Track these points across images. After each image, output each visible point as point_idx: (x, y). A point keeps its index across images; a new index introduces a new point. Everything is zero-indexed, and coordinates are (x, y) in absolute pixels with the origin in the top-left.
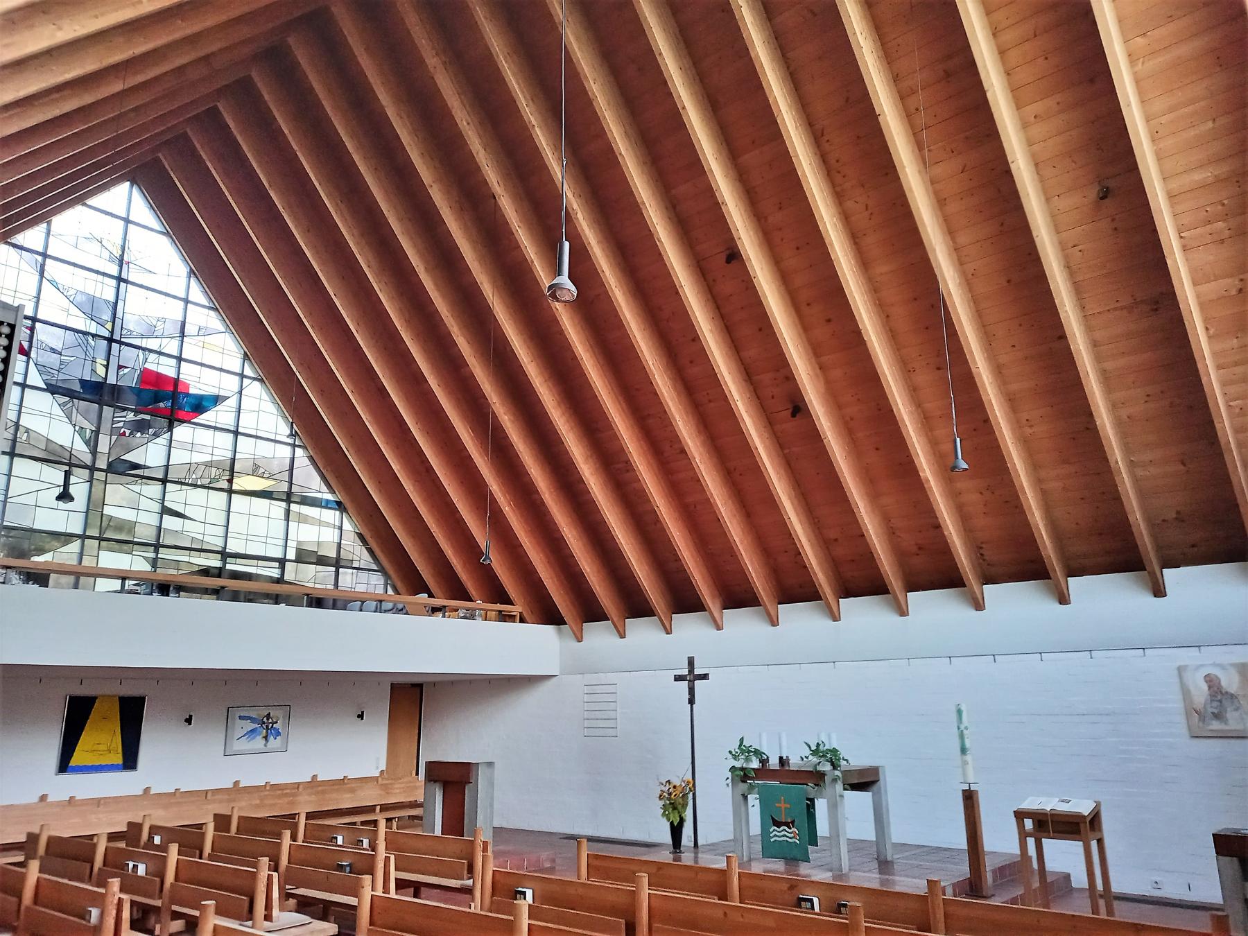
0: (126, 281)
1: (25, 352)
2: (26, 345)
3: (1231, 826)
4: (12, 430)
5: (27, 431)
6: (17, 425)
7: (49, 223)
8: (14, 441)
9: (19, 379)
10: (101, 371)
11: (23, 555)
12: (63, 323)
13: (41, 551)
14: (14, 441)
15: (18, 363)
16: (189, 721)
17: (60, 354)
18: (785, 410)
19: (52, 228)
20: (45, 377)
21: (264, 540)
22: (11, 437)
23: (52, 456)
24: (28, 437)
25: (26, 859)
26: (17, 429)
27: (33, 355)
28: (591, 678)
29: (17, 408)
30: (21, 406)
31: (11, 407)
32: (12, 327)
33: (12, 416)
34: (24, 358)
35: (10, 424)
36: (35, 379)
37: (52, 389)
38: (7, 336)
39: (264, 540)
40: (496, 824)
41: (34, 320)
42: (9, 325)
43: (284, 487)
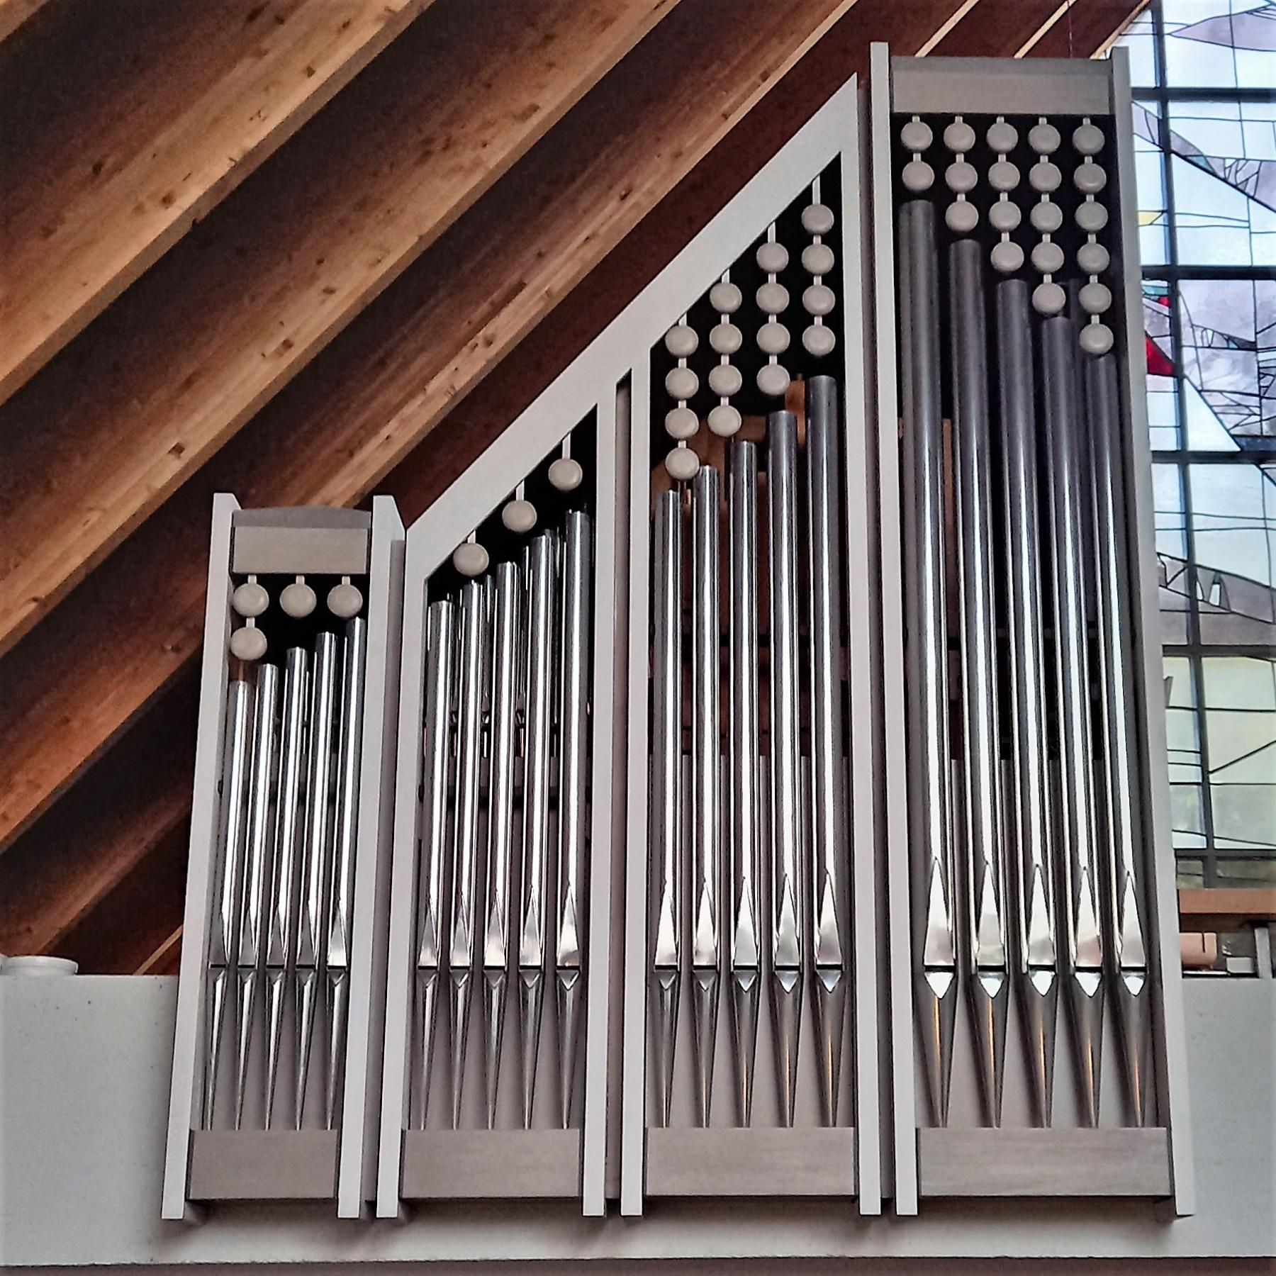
0: (1258, 396)
1: (1165, 365)
2: (1165, 345)
4: (1180, 584)
5: (1218, 577)
6: (1190, 565)
8: (1193, 611)
9: (1168, 442)
12: (1242, 261)
14: (1193, 611)
17: (1251, 347)
20: (1230, 420)
21: (1261, 524)
22: (1181, 602)
26: (1192, 581)
27: (1191, 372)
28: (423, 137)
29: (1178, 521)
30: (1187, 513)
31: (1160, 521)
32: (1106, 124)
33: (1171, 545)
34: (1169, 382)
38: (1106, 318)
39: (1261, 524)
40: (1153, 448)
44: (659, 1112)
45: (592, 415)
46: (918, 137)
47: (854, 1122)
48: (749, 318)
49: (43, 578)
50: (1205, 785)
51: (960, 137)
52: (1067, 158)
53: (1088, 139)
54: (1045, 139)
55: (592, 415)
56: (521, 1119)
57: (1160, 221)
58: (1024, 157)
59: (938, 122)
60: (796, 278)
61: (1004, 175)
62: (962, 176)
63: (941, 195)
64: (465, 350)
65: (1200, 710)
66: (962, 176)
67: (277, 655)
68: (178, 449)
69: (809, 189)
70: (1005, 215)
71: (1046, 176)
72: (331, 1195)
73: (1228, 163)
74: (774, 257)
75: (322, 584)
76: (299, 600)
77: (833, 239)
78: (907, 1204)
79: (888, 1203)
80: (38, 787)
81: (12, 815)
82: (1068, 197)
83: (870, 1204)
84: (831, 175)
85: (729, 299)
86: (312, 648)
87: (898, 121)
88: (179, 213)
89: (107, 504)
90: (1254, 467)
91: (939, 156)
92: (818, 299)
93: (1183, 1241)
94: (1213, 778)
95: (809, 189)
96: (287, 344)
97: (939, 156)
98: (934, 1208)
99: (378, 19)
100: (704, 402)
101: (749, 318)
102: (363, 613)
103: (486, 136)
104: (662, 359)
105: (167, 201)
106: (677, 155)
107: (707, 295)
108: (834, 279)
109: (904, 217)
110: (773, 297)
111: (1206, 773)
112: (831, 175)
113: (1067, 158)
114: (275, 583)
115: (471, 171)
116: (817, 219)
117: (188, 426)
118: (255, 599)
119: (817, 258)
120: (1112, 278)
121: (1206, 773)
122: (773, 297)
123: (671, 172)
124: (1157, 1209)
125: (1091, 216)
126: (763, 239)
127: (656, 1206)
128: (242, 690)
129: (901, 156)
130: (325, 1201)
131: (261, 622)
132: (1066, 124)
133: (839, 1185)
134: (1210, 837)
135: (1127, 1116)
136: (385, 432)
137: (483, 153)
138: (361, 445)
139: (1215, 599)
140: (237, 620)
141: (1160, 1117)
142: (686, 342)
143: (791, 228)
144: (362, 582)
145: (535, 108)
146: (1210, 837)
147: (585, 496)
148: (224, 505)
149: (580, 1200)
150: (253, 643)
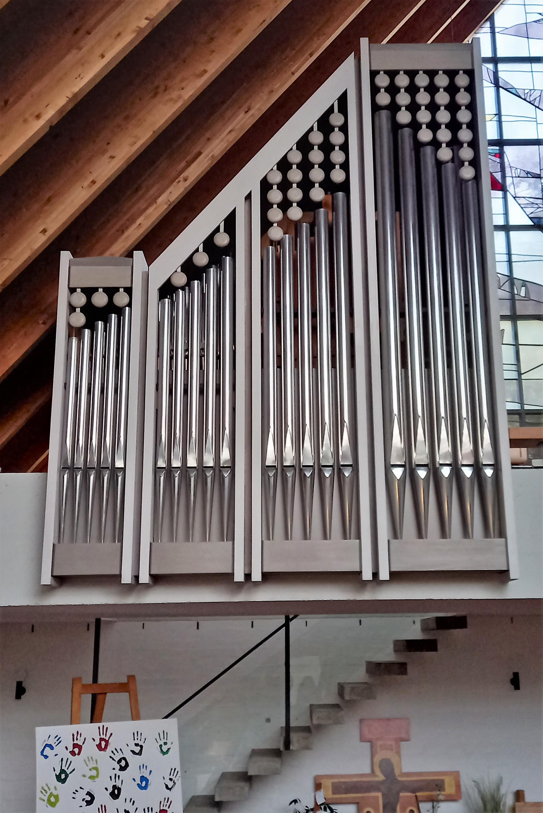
1: (499, 186)
2: (498, 176)
3: (155, 623)
4: (507, 287)
5: (525, 283)
6: (511, 279)
7: (491, 19)
8: (513, 300)
9: (499, 221)
15: (495, 202)
16: (515, 682)
18: (187, 373)
19: (497, 24)
20: (529, 210)
22: (507, 295)
24: (527, 291)
25: (120, 766)
26: (512, 285)
27: (511, 189)
30: (509, 254)
32: (470, 73)
34: (500, 194)
35: (503, 279)
36: (518, 217)
41: (495, 60)
42: (466, 72)
43: (435, 804)
44: (396, 532)
46: (383, 81)
47: (359, 537)
48: (306, 166)
50: (519, 380)
51: (402, 81)
52: (452, 89)
53: (462, 81)
54: (442, 81)
58: (432, 89)
59: (392, 74)
60: (327, 147)
61: (423, 98)
62: (403, 99)
64: (175, 183)
65: (516, 345)
66: (403, 99)
67: (91, 325)
68: (44, 231)
71: (442, 98)
72: (118, 573)
74: (317, 138)
75: (111, 292)
76: (100, 300)
77: (344, 129)
78: (384, 575)
84: (343, 100)
85: (296, 157)
86: (107, 321)
87: (374, 74)
89: (12, 256)
91: (393, 90)
92: (337, 157)
93: (514, 591)
96: (94, 182)
97: (393, 90)
99: (133, 31)
100: (285, 205)
101: (306, 166)
102: (130, 305)
103: (183, 85)
104: (266, 186)
105: (38, 117)
107: (285, 156)
108: (345, 147)
112: (343, 100)
113: (452, 89)
114: (89, 292)
115: (176, 101)
116: (336, 119)
118: (80, 299)
120: (474, 144)
122: (316, 156)
124: (501, 576)
125: (463, 98)
127: (267, 577)
128: (74, 341)
129: (375, 90)
131: (83, 310)
132: (452, 74)
133: (351, 566)
135: (487, 533)
136: (138, 221)
139: (523, 294)
141: (502, 534)
143: (324, 124)
144: (129, 291)
145: (205, 71)
148: (65, 256)
149: (120, 576)
150: (79, 319)
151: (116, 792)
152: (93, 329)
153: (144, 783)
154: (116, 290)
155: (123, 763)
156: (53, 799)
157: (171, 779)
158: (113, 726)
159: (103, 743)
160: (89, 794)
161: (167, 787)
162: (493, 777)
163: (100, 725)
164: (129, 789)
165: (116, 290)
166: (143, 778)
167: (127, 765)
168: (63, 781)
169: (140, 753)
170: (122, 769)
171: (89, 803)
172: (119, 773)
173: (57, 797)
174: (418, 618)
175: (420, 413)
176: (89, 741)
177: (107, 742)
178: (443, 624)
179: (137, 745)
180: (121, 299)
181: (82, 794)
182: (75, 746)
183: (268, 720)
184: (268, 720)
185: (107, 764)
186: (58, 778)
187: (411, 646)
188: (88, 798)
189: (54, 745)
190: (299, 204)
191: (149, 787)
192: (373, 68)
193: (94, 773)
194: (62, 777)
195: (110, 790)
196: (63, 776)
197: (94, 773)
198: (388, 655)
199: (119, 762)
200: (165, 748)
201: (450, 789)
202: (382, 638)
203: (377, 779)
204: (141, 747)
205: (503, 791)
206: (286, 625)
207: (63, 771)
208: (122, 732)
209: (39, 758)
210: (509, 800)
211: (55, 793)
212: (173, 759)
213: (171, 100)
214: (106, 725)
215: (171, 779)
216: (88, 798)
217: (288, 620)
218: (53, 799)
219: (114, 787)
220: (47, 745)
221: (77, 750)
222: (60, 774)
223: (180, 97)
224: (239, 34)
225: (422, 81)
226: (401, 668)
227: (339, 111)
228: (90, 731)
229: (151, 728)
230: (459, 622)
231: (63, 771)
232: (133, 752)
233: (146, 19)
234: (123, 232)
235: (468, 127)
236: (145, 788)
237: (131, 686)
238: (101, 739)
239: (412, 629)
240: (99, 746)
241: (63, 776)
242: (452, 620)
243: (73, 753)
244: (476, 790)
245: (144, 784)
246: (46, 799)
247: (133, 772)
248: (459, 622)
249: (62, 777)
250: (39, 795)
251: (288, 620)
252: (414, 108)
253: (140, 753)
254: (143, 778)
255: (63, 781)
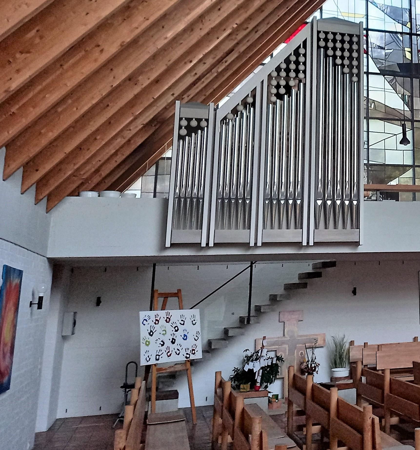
10: (408, 55)
11: (382, 181)
13: (392, 178)
16: (354, 292)
23: (389, 116)
32: (358, 36)
36: (373, 68)
37: (383, 72)
45: (256, 88)
46: (322, 36)
47: (302, 228)
48: (288, 70)
49: (144, 120)
50: (368, 149)
51: (330, 37)
52: (351, 43)
53: (355, 39)
55: (256, 88)
56: (237, 228)
57: (365, 17)
58: (342, 42)
59: (326, 33)
60: (297, 63)
61: (339, 45)
62: (330, 44)
63: (326, 48)
64: (221, 63)
65: (368, 132)
66: (330, 44)
68: (173, 94)
69: (300, 45)
70: (338, 53)
72: (248, 242)
73: (381, 5)
74: (293, 58)
75: (199, 120)
76: (194, 123)
77: (305, 55)
79: (207, 244)
80: (123, 155)
81: (118, 161)
82: (351, 50)
83: (204, 244)
84: (305, 42)
85: (284, 66)
86: (196, 133)
87: (319, 32)
88: (193, 64)
89: (158, 105)
90: (382, 76)
92: (301, 67)
93: (360, 249)
94: (370, 147)
95: (300, 45)
96: (196, 74)
97: (326, 40)
98: (316, 244)
99: (231, 29)
100: (278, 87)
101: (288, 70)
102: (207, 127)
103: (238, 33)
105: (191, 62)
106: (268, 23)
107: (279, 65)
108: (305, 64)
109: (319, 51)
110: (293, 66)
111: (368, 146)
112: (305, 42)
113: (351, 43)
114: (189, 120)
115: (234, 40)
116: (302, 51)
117: (175, 90)
118: (184, 123)
119: (302, 59)
121: (368, 146)
122: (293, 66)
123: (267, 27)
125: (355, 63)
126: (291, 54)
127: (173, 245)
128: (181, 141)
129: (319, 39)
130: (248, 243)
131: (186, 127)
132: (351, 36)
133: (298, 240)
134: (368, 161)
135: (352, 227)
136: (202, 80)
137: (237, 37)
138: (197, 83)
139: (373, 107)
140: (180, 127)
141: (358, 227)
142: (275, 74)
143: (296, 52)
144: (207, 120)
145: (247, 28)
146: (368, 161)
147: (253, 104)
148: (178, 103)
149: (201, 243)
150: (184, 132)
151: (174, 341)
152: (190, 136)
153: (185, 338)
154: (201, 120)
155: (176, 328)
156: (147, 343)
157: (197, 336)
158: (172, 312)
159: (168, 319)
160: (162, 341)
161: (195, 340)
162: (341, 336)
163: (167, 311)
164: (179, 340)
165: (201, 120)
166: (185, 335)
167: (178, 329)
168: (152, 335)
169: (183, 324)
170: (176, 331)
171: (162, 345)
172: (175, 333)
173: (149, 342)
174: (311, 262)
175: (330, 179)
176: (162, 318)
177: (169, 319)
178: (325, 265)
179: (182, 320)
180: (204, 124)
181: (159, 342)
182: (156, 320)
183: (233, 314)
184: (233, 314)
185: (170, 329)
186: (149, 334)
187: (309, 275)
188: (162, 343)
189: (147, 320)
190: (284, 87)
191: (187, 339)
192: (319, 30)
193: (164, 332)
194: (151, 334)
195: (171, 340)
196: (151, 333)
197: (164, 332)
198: (280, 291)
199: (175, 328)
200: (194, 322)
201: (320, 342)
202: (293, 272)
203: (286, 339)
204: (184, 321)
205: (345, 341)
206: (251, 266)
207: (151, 331)
208: (176, 314)
209: (141, 325)
210: (347, 346)
211: (148, 340)
212: (198, 327)
213: (232, 39)
214: (169, 311)
215: (197, 336)
216: (162, 343)
217: (252, 263)
218: (147, 343)
219: (173, 339)
220: (145, 320)
221: (157, 322)
222: (150, 332)
223: (236, 38)
224: (263, 12)
225: (339, 37)
226: (305, 285)
227: (303, 47)
228: (162, 314)
229: (187, 313)
230: (333, 264)
231: (151, 331)
232: (180, 323)
233: (236, 24)
234: (195, 85)
235: (356, 51)
236: (186, 339)
237: (179, 295)
238: (167, 318)
239: (307, 267)
240: (166, 321)
241: (151, 333)
242: (329, 263)
243: (155, 323)
244: (333, 341)
245: (185, 338)
246: (144, 342)
247: (180, 333)
248: (333, 264)
249: (151, 334)
250: (141, 341)
251: (252, 263)
252: (334, 49)
253: (183, 324)
254: (185, 335)
255: (152, 335)
